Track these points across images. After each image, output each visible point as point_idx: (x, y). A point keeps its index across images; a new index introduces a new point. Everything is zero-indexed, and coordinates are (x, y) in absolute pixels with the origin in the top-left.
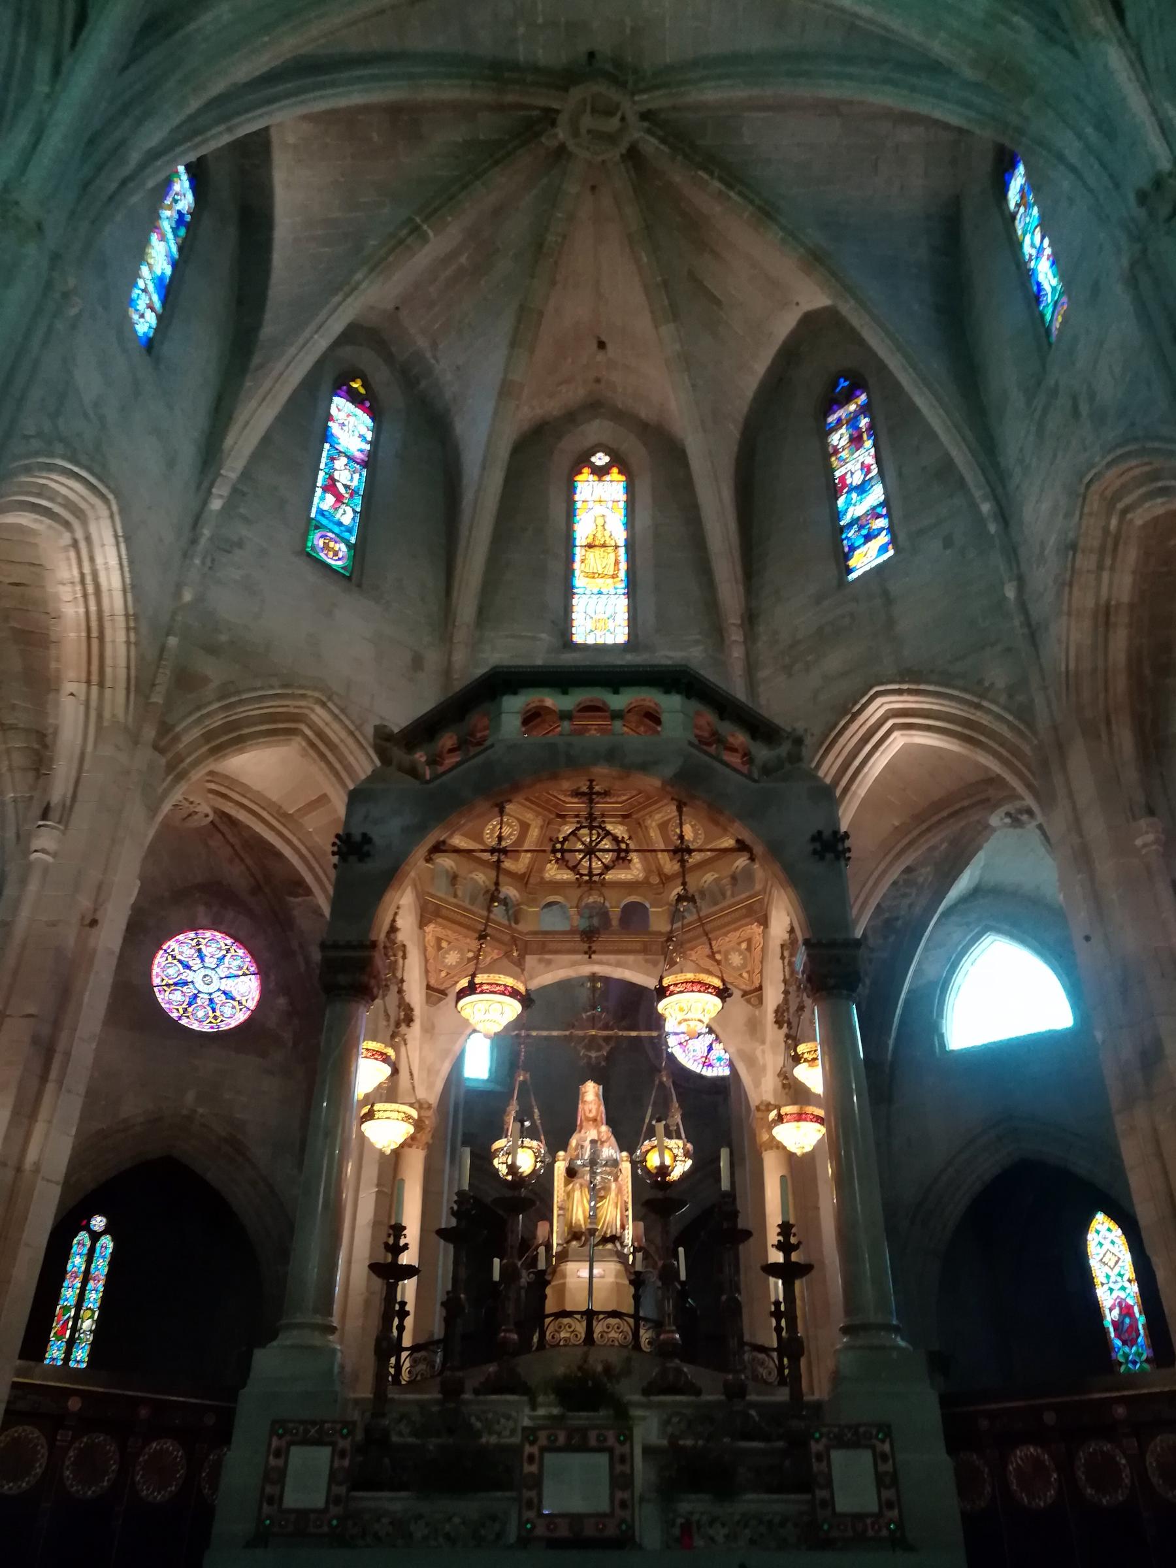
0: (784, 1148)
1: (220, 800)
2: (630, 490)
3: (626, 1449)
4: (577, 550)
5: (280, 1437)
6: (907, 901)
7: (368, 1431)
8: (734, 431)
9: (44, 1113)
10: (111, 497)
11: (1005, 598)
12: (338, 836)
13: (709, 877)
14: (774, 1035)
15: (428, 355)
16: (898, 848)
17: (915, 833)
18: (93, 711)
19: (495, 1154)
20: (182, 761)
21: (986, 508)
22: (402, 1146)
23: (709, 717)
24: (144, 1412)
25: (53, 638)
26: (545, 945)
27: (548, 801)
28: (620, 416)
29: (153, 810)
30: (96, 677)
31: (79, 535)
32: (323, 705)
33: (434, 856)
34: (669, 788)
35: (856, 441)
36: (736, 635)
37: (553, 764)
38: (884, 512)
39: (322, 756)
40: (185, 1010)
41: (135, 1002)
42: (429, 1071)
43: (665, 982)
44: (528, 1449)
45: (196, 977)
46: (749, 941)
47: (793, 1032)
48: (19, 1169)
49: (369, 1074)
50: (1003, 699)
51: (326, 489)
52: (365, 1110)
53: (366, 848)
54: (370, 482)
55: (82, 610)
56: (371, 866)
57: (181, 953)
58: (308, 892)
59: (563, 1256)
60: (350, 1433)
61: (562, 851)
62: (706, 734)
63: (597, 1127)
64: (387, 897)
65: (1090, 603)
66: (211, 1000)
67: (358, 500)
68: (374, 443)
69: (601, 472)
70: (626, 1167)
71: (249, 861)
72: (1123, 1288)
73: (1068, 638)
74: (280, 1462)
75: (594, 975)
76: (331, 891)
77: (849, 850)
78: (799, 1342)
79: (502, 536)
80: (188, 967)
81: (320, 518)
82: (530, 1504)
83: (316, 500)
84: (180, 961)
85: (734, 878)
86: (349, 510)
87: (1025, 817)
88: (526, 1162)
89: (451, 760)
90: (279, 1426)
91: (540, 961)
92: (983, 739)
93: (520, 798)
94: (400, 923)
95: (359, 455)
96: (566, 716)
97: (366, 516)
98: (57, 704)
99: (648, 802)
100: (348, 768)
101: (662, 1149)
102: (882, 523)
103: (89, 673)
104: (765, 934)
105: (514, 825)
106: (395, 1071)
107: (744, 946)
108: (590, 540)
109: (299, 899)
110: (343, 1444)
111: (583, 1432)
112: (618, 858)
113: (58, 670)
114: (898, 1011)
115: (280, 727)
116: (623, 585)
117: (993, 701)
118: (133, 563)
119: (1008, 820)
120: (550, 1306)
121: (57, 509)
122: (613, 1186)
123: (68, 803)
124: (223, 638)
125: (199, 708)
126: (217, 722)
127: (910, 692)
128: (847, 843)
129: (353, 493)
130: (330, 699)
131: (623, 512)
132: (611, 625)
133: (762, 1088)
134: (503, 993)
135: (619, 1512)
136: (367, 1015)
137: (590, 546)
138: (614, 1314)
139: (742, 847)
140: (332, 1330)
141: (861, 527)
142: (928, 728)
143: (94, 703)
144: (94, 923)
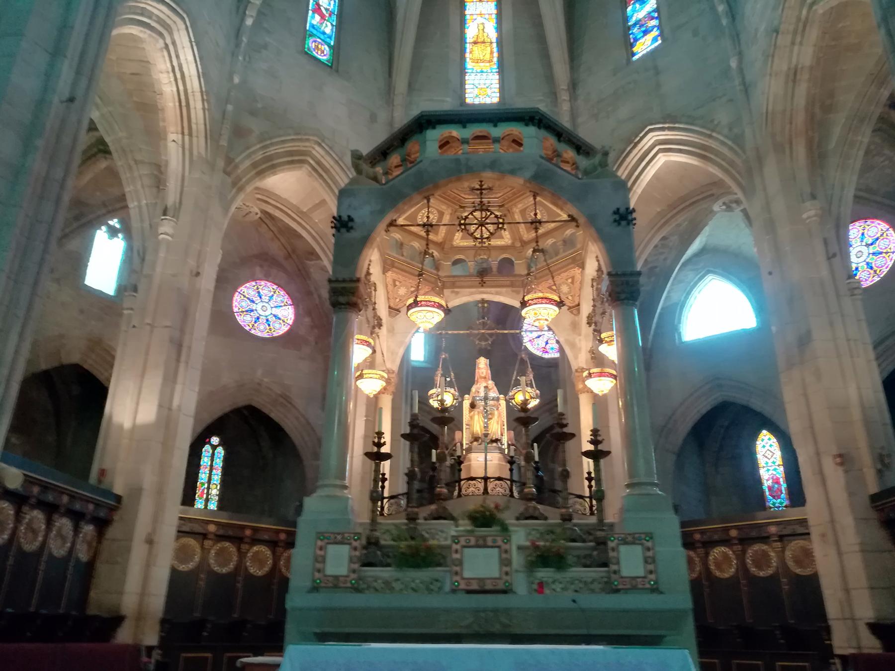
0: (592, 392)
1: (264, 204)
3: (507, 547)
4: (468, 46)
5: (322, 540)
6: (662, 257)
7: (368, 538)
9: (180, 379)
10: (185, 16)
11: (729, 66)
12: (334, 217)
13: (550, 241)
14: (587, 331)
16: (659, 225)
17: (669, 216)
18: (187, 151)
19: (431, 396)
20: (240, 180)
22: (379, 393)
23: (552, 140)
25: (160, 107)
26: (454, 284)
27: (454, 198)
29: (226, 209)
30: (187, 129)
31: (169, 41)
32: (320, 145)
33: (392, 229)
34: (528, 185)
36: (564, 96)
37: (459, 170)
38: (656, 15)
39: (321, 176)
40: (253, 326)
41: (224, 321)
42: (392, 354)
43: (526, 299)
44: (455, 547)
45: (258, 307)
46: (573, 278)
47: (598, 328)
48: (170, 409)
49: (359, 353)
50: (726, 131)
51: (314, 11)
52: (358, 373)
53: (350, 224)
55: (175, 89)
56: (355, 234)
57: (248, 294)
58: (318, 258)
59: (469, 450)
60: (359, 539)
61: (465, 224)
62: (550, 153)
63: (486, 381)
64: (364, 253)
65: (785, 67)
66: (267, 320)
67: (334, 18)
69: (113, 232)
70: (503, 403)
71: (283, 240)
72: (775, 470)
73: (770, 90)
74: (322, 553)
75: (483, 299)
76: (331, 258)
77: (635, 219)
78: (602, 492)
80: (253, 302)
81: (312, 30)
82: (456, 573)
83: (309, 18)
84: (248, 299)
85: (565, 242)
86: (329, 24)
87: (734, 205)
88: (449, 399)
89: (397, 172)
90: (320, 535)
91: (452, 292)
92: (712, 156)
93: (438, 193)
94: (371, 271)
96: (465, 141)
98: (166, 146)
99: (516, 196)
100: (335, 182)
101: (524, 392)
103: (183, 128)
104: (582, 274)
105: (437, 210)
106: (374, 352)
107: (570, 281)
108: (475, 39)
109: (312, 263)
110: (355, 544)
111: (484, 538)
112: (498, 227)
113: (165, 127)
114: (655, 320)
115: (295, 159)
116: (496, 67)
117: (719, 133)
118: (203, 58)
119: (724, 207)
120: (463, 475)
121: (154, 24)
122: (496, 412)
123: (177, 205)
124: (259, 106)
125: (248, 148)
126: (259, 156)
127: (669, 129)
128: (634, 215)
130: (323, 141)
131: (495, 21)
132: (489, 91)
133: (579, 359)
134: (433, 306)
135: (505, 577)
136: (358, 320)
137: (475, 43)
138: (499, 479)
140: (346, 487)
141: (642, 26)
142: (680, 151)
143: (187, 146)
144: (198, 274)
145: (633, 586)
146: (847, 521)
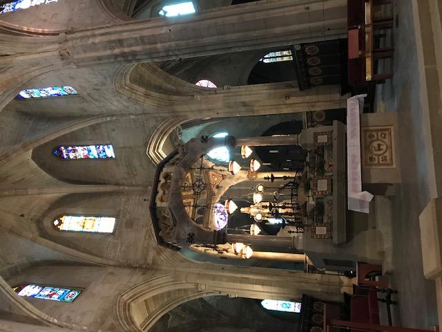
2: (68, 215)
8: (60, 183)
11: (133, 119)
15: (10, 266)
21: (108, 119)
24: (306, 321)
28: (44, 215)
35: (75, 151)
56: (196, 233)
69: (61, 223)
73: (149, 105)
79: (77, 248)
95: (40, 288)
97: (61, 287)
115: (127, 307)
124: (99, 320)
129: (53, 290)
137: (84, 227)
139: (202, 156)
145: (330, 139)
146: (308, 98)
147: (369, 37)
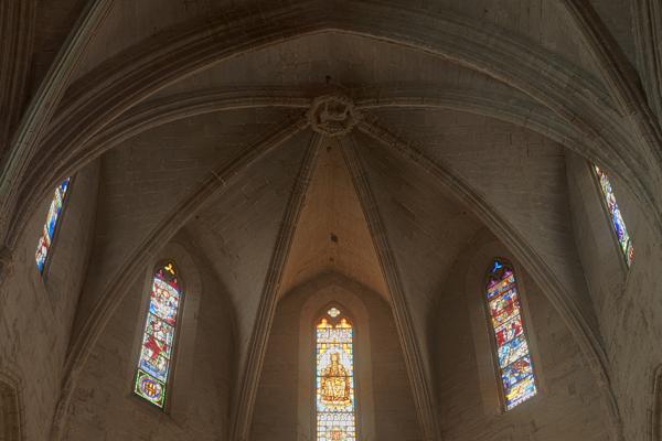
4: (319, 379)
35: (508, 308)
51: (147, 345)
54: (177, 337)
68: (180, 309)
69: (334, 322)
81: (144, 367)
102: (528, 369)
137: (328, 376)
147: (34, 250)
